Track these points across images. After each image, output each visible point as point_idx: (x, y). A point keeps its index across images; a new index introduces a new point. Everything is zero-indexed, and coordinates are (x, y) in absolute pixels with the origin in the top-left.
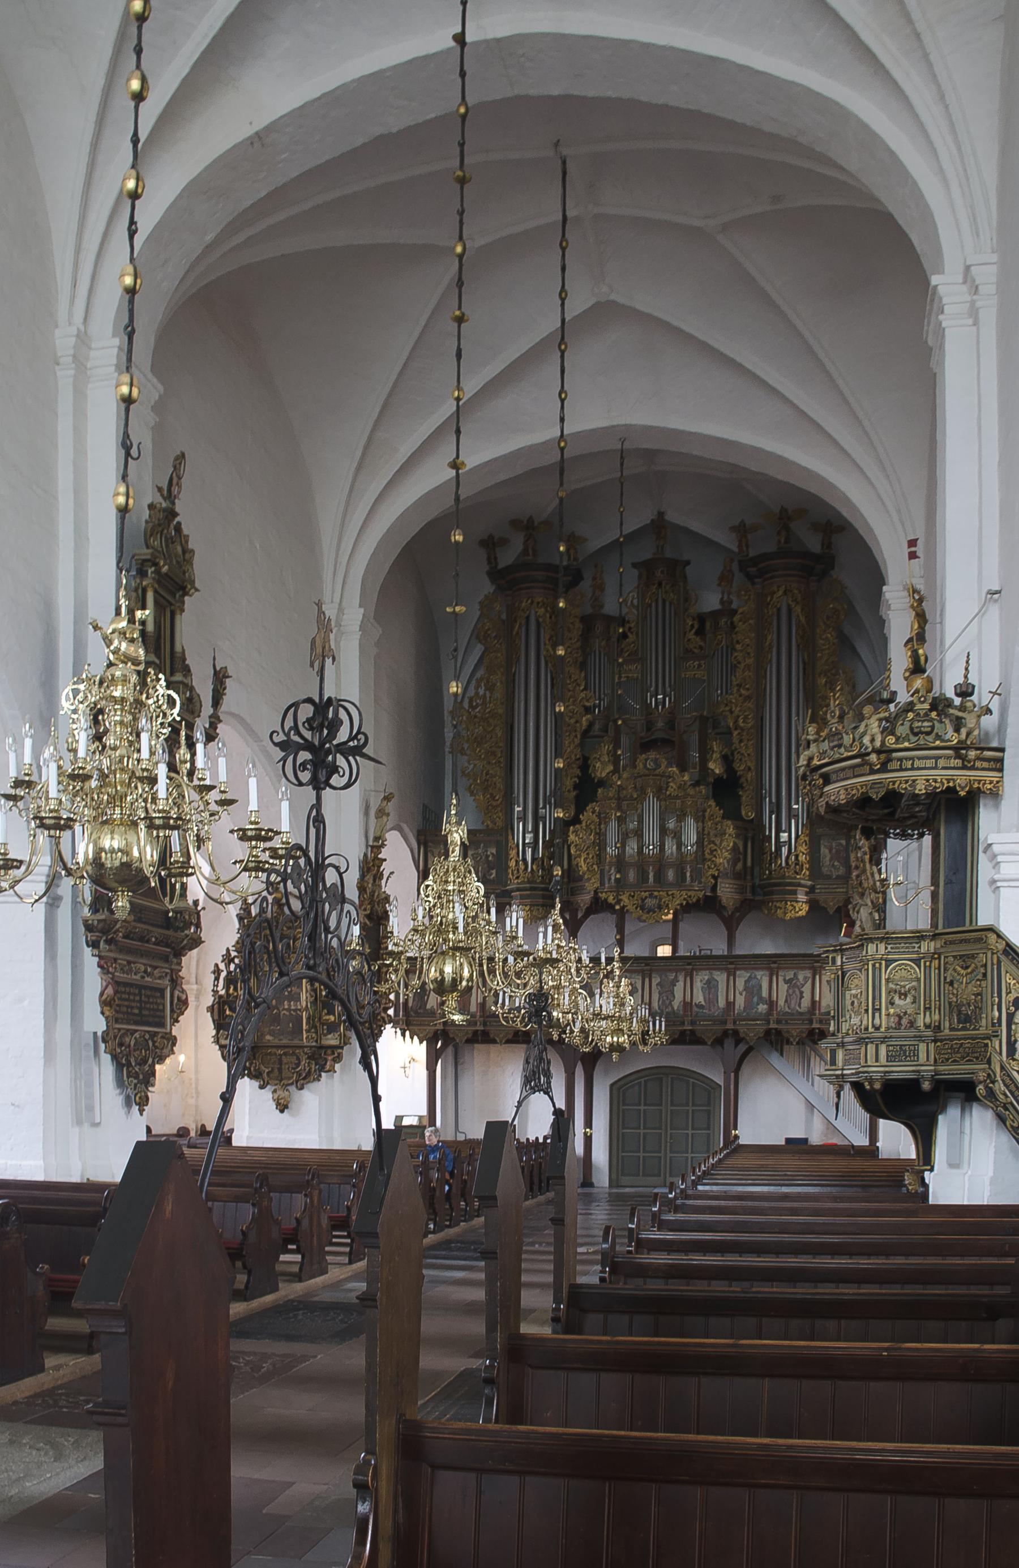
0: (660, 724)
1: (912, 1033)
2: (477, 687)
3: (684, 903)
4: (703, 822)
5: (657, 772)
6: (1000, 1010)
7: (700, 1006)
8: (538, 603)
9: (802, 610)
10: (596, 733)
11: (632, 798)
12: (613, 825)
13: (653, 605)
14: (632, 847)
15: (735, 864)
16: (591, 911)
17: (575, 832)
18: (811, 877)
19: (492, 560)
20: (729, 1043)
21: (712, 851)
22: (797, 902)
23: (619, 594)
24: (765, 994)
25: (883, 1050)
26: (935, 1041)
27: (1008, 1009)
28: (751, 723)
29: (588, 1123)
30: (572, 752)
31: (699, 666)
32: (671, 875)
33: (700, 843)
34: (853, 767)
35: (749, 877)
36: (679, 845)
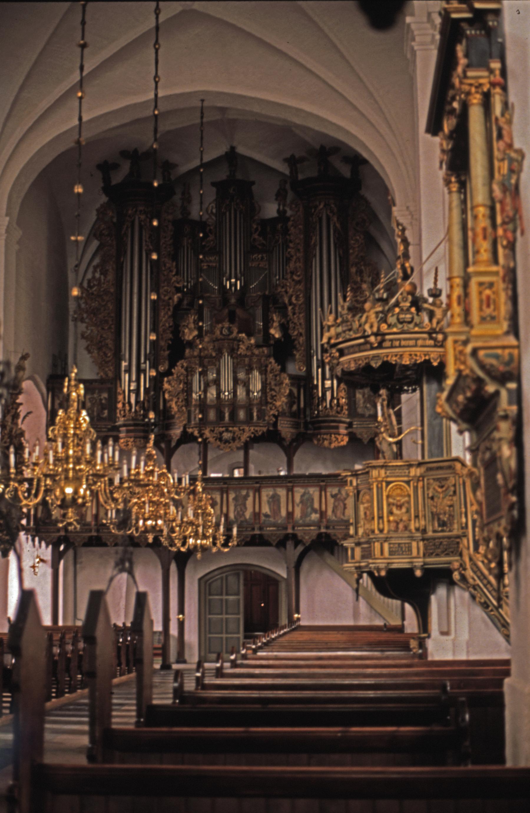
0: (233, 301)
1: (407, 534)
2: (94, 272)
3: (253, 436)
4: (266, 374)
5: (231, 337)
6: (466, 516)
7: (266, 516)
8: (141, 211)
9: (338, 218)
10: (185, 307)
11: (211, 356)
12: (196, 377)
13: (228, 214)
14: (212, 393)
15: (291, 406)
16: (180, 442)
17: (169, 382)
18: (350, 415)
19: (106, 179)
20: (290, 545)
21: (273, 397)
22: (339, 434)
23: (202, 205)
24: (316, 505)
25: (386, 546)
26: (423, 540)
27: (472, 516)
28: (302, 300)
29: (181, 610)
30: (166, 321)
31: (262, 258)
32: (242, 414)
33: (264, 390)
34: (360, 345)
35: (302, 416)
36: (248, 392)
